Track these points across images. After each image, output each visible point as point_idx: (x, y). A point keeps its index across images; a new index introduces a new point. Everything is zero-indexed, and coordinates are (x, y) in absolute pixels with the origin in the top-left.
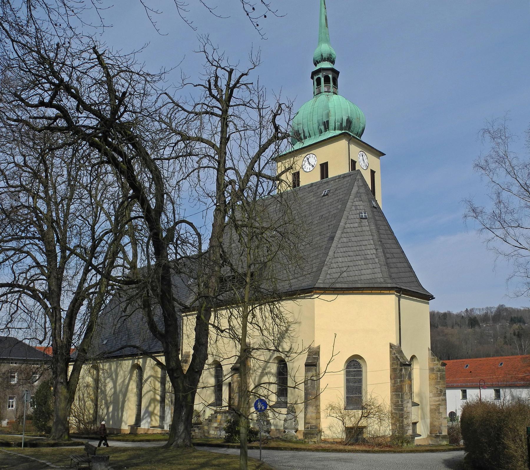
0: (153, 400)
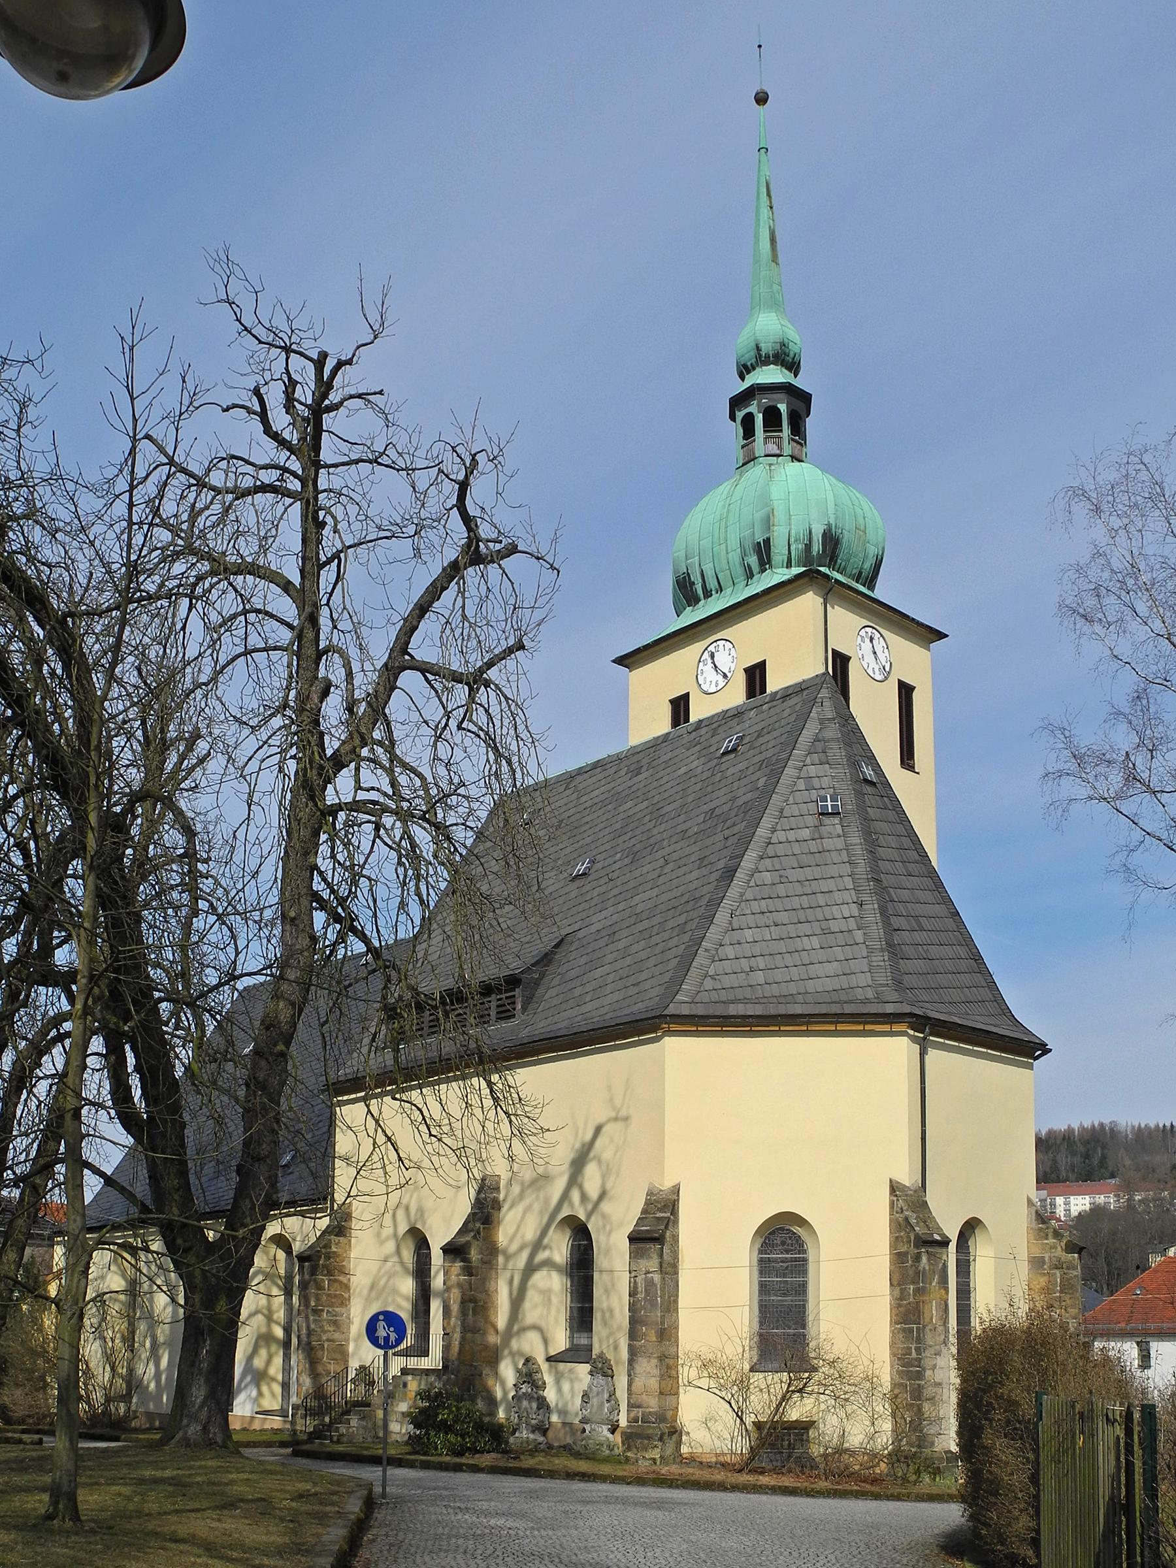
0: (265, 1339)
